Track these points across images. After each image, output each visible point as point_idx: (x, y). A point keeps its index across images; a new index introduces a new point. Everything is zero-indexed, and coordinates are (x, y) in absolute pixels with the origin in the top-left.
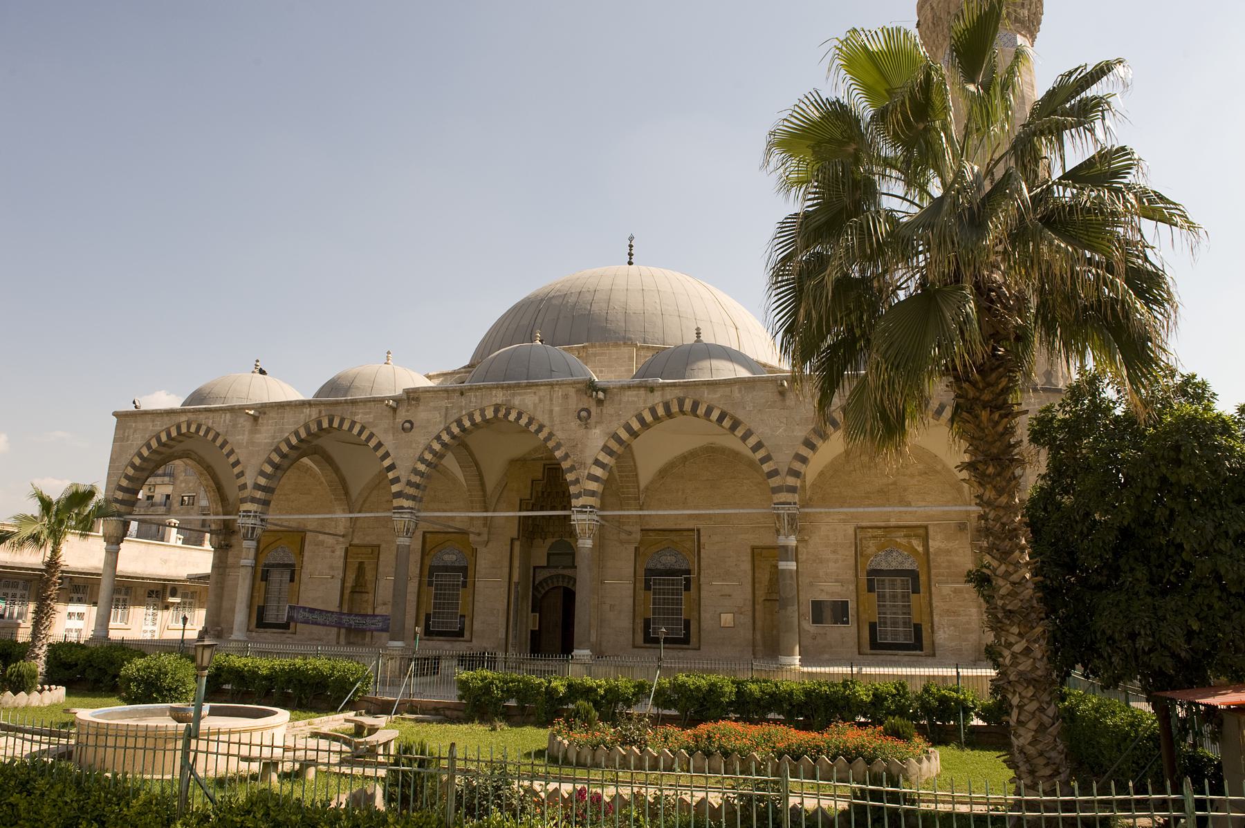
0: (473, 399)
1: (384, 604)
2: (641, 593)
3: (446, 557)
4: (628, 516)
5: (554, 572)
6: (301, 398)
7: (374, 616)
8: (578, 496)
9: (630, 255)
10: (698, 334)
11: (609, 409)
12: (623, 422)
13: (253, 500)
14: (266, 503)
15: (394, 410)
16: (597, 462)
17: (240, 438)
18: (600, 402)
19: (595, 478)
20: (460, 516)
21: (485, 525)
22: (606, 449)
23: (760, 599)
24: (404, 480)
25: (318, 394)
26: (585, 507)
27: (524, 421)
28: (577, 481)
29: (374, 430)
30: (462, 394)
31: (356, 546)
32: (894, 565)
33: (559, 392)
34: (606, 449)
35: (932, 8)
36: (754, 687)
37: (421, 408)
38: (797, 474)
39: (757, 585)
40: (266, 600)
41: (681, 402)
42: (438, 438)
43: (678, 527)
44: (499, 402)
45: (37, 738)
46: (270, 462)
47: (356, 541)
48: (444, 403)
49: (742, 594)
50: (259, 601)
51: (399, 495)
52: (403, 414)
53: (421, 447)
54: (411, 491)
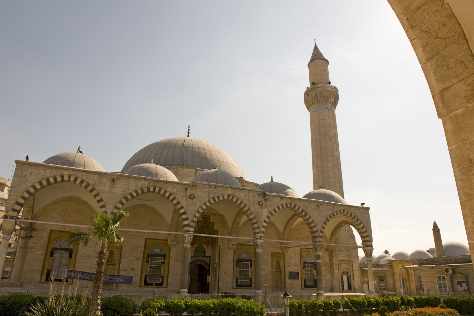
0: (220, 191)
1: (124, 270)
2: (302, 269)
3: (155, 250)
4: (232, 239)
5: (197, 258)
6: (103, 170)
7: (118, 276)
8: (259, 233)
9: (189, 133)
10: (272, 178)
11: (269, 203)
12: (273, 208)
15: (186, 189)
16: (265, 221)
17: (104, 187)
18: (266, 200)
20: (163, 233)
21: (175, 237)
23: (274, 271)
24: (190, 219)
25: (305, 196)
26: (261, 237)
27: (239, 202)
29: (176, 196)
30: (215, 187)
32: (310, 261)
33: (251, 194)
35: (315, 93)
36: (372, 300)
37: (198, 190)
38: (322, 232)
41: (69, 177)
42: (205, 204)
44: (230, 193)
48: (208, 190)
51: (188, 225)
52: (189, 192)
53: (198, 206)
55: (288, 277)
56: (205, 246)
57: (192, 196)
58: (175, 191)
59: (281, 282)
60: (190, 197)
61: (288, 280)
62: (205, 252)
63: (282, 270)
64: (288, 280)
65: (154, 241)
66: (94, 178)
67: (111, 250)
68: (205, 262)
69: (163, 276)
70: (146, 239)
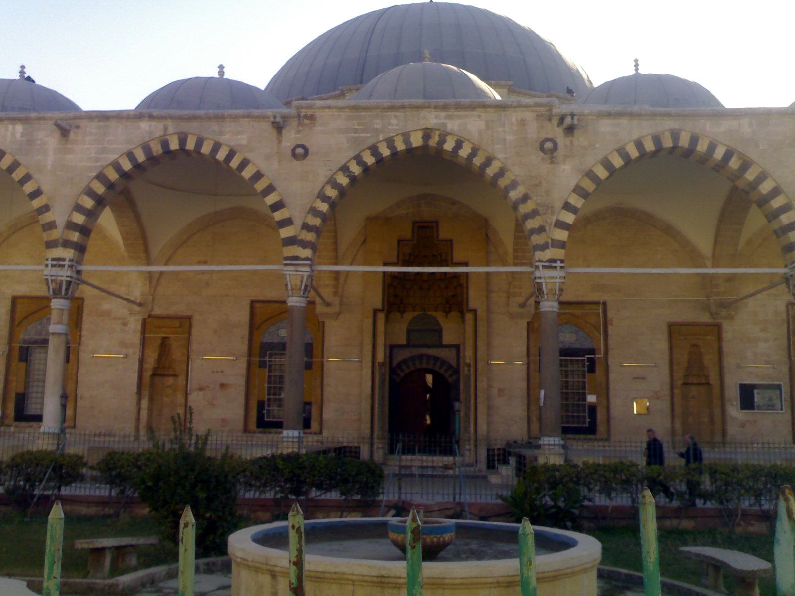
1: (201, 389)
8: (543, 247)
10: (636, 66)
11: (580, 139)
13: (66, 244)
14: (81, 249)
16: (567, 206)
19: (560, 225)
22: (579, 190)
24: (298, 223)
26: (555, 261)
28: (541, 230)
29: (250, 156)
31: (158, 317)
34: (579, 190)
37: (318, 128)
39: (675, 368)
40: (27, 384)
43: (580, 299)
45: (634, 449)
46: (91, 193)
47: (157, 311)
49: (659, 378)
50: (17, 386)
51: (291, 241)
52: (291, 137)
54: (310, 237)
55: (737, 402)
56: (439, 316)
57: (300, 151)
58: (244, 142)
59: (712, 421)
60: (294, 155)
61: (735, 411)
62: (439, 332)
63: (713, 379)
64: (735, 411)
65: (277, 305)
66: (13, 134)
67: (164, 339)
68: (444, 362)
69: (310, 404)
70: (253, 303)
